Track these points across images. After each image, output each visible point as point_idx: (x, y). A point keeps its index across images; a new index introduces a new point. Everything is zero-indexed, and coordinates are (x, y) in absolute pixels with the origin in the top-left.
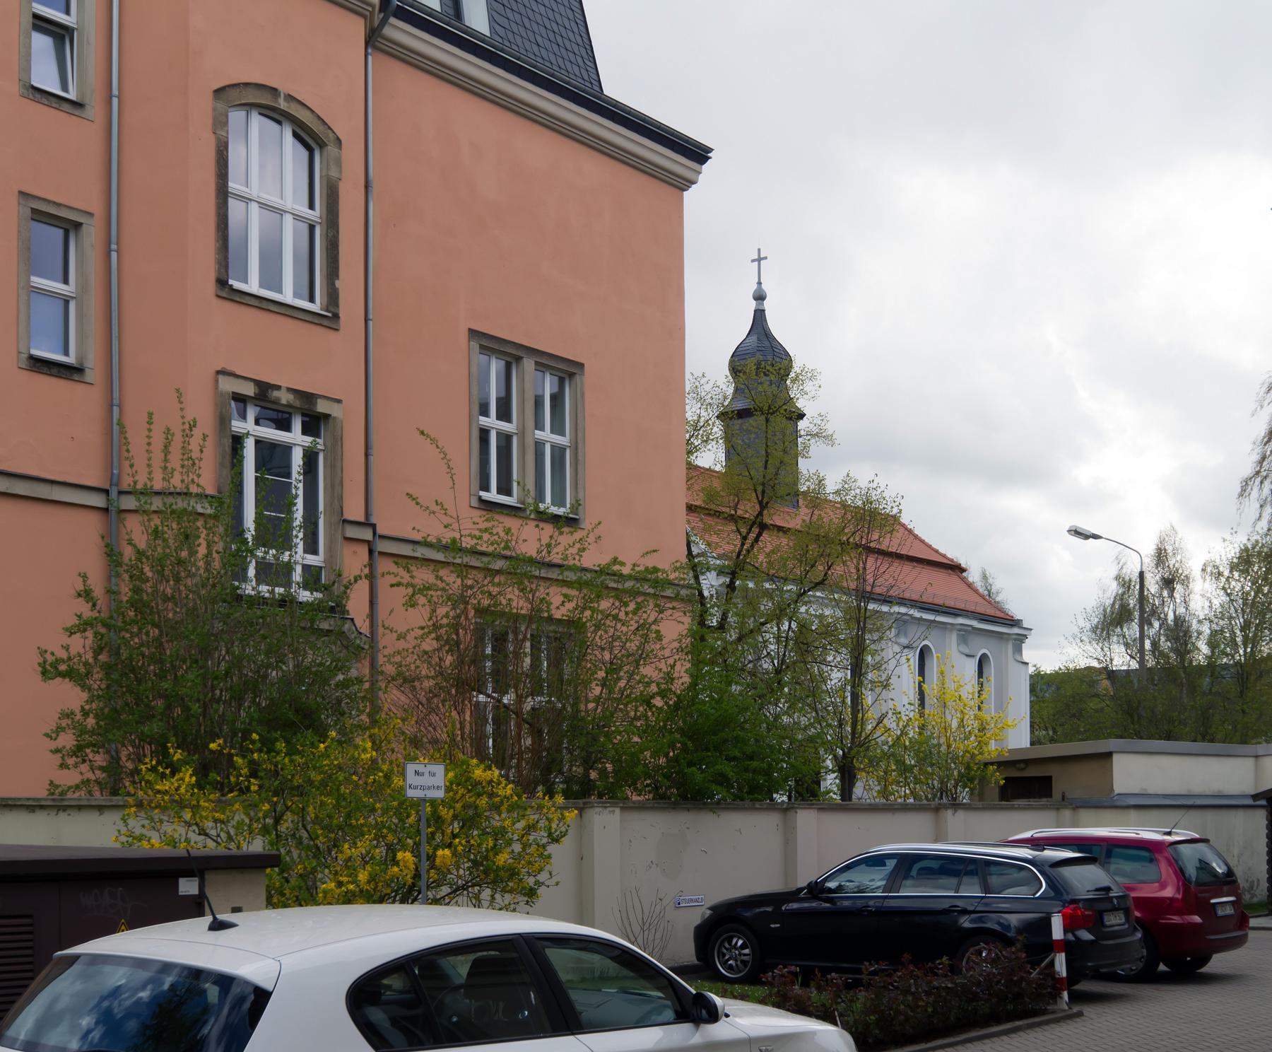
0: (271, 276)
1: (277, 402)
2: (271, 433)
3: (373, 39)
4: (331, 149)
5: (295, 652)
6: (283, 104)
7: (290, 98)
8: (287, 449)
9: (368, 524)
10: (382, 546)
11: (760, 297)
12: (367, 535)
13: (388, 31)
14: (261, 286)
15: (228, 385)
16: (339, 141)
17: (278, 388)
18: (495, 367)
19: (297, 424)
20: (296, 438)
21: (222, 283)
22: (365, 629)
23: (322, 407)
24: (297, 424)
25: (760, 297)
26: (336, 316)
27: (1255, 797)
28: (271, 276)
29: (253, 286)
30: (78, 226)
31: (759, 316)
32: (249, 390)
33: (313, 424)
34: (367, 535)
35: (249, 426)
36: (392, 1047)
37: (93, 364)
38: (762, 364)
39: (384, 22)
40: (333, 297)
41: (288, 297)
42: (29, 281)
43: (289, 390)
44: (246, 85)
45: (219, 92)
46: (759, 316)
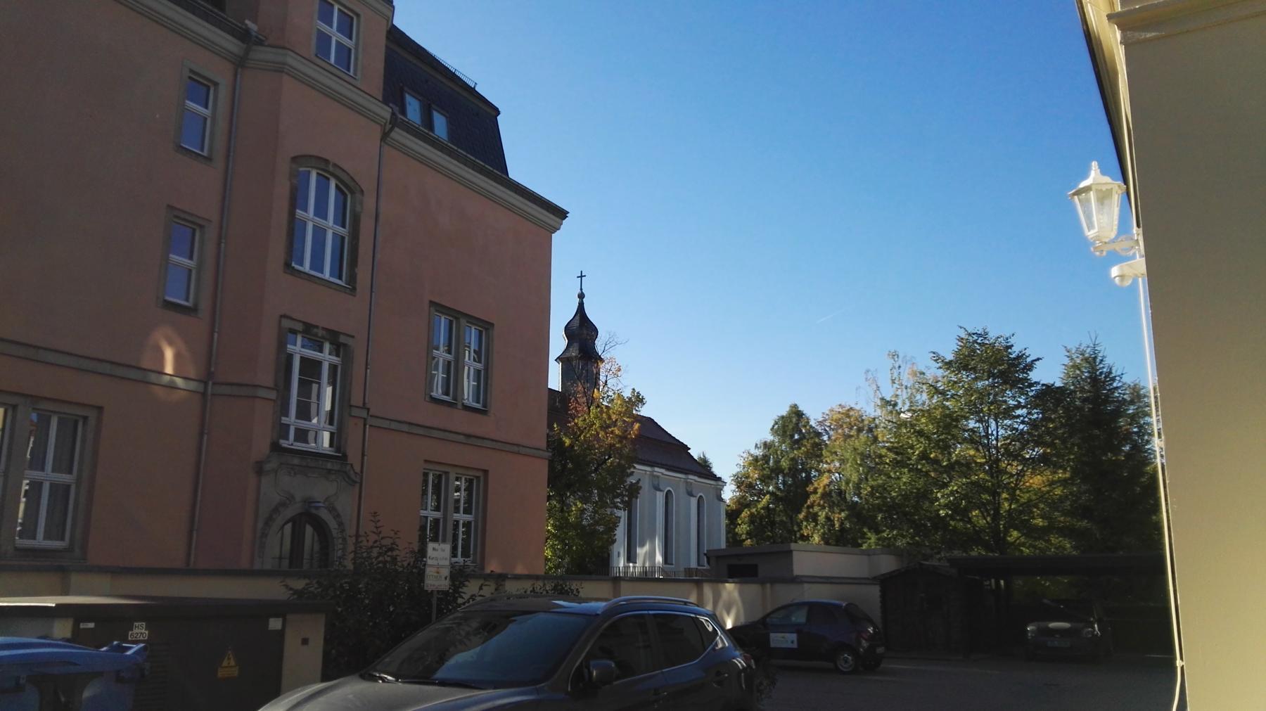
0: (317, 263)
1: (316, 335)
2: (311, 354)
3: (385, 136)
4: (358, 195)
5: (779, 489)
6: (331, 169)
7: (335, 165)
8: (319, 363)
9: (364, 406)
10: (371, 421)
11: (581, 296)
12: (364, 414)
13: (393, 135)
14: (311, 268)
15: (287, 324)
16: (362, 191)
17: (317, 327)
18: (443, 320)
19: (327, 346)
20: (327, 357)
21: (288, 265)
22: (358, 469)
23: (342, 339)
24: (327, 346)
25: (581, 296)
26: (354, 289)
27: (875, 578)
28: (317, 263)
29: (307, 267)
30: (201, 227)
31: (581, 306)
32: (299, 327)
33: (338, 348)
34: (364, 414)
35: (298, 349)
36: (223, 10)
37: (205, 305)
38: (582, 331)
39: (391, 130)
40: (352, 279)
41: (327, 275)
42: (168, 258)
43: (324, 329)
44: (311, 156)
45: (295, 159)
46: (581, 306)
